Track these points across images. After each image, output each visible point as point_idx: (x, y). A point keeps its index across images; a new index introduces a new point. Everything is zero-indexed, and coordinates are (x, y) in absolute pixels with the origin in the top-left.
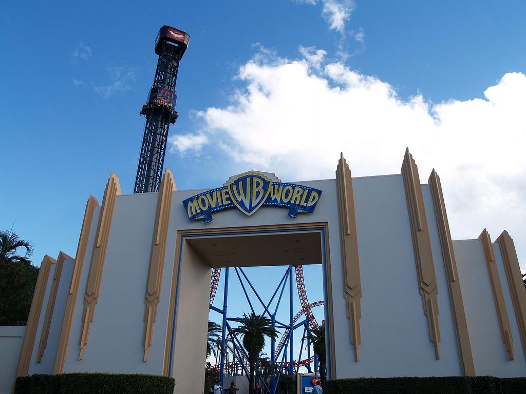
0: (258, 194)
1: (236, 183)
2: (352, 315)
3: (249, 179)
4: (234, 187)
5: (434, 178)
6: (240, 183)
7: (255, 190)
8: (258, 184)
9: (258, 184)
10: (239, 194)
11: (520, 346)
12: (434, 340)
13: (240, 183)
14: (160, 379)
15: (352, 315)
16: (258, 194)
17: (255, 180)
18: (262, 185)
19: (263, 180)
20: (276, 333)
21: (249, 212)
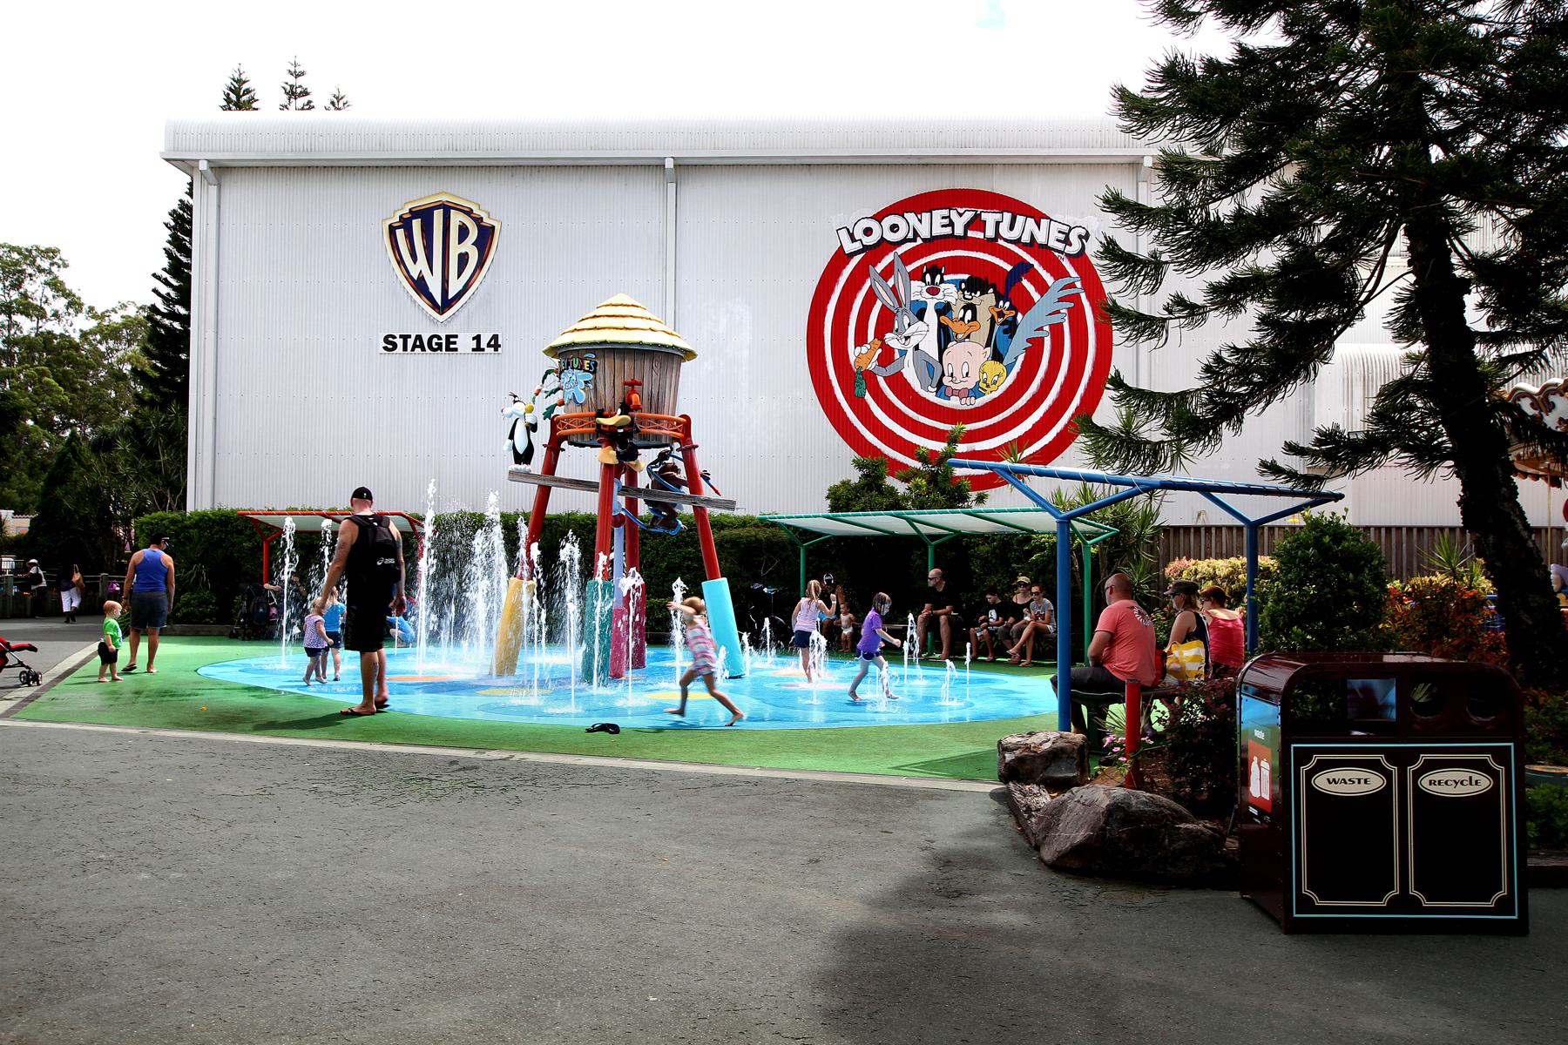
0: (463, 259)
1: (406, 224)
2: (416, 778)
3: (438, 216)
4: (400, 233)
5: (1028, 340)
6: (416, 224)
7: (455, 250)
8: (463, 232)
9: (463, 232)
10: (861, 339)
11: (868, 432)
12: (1038, 504)
13: (416, 224)
14: (1553, 486)
15: (416, 778)
16: (463, 259)
17: (456, 218)
18: (474, 234)
19: (478, 220)
20: (1408, 344)
21: (442, 313)
